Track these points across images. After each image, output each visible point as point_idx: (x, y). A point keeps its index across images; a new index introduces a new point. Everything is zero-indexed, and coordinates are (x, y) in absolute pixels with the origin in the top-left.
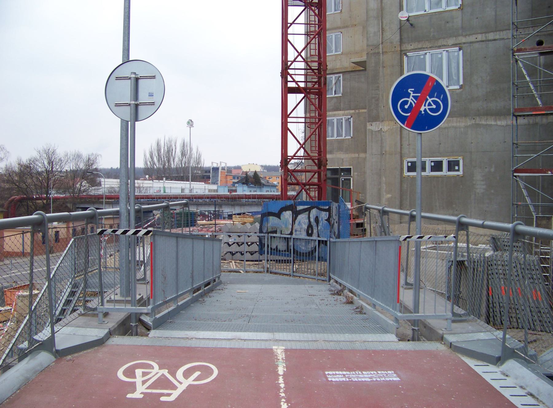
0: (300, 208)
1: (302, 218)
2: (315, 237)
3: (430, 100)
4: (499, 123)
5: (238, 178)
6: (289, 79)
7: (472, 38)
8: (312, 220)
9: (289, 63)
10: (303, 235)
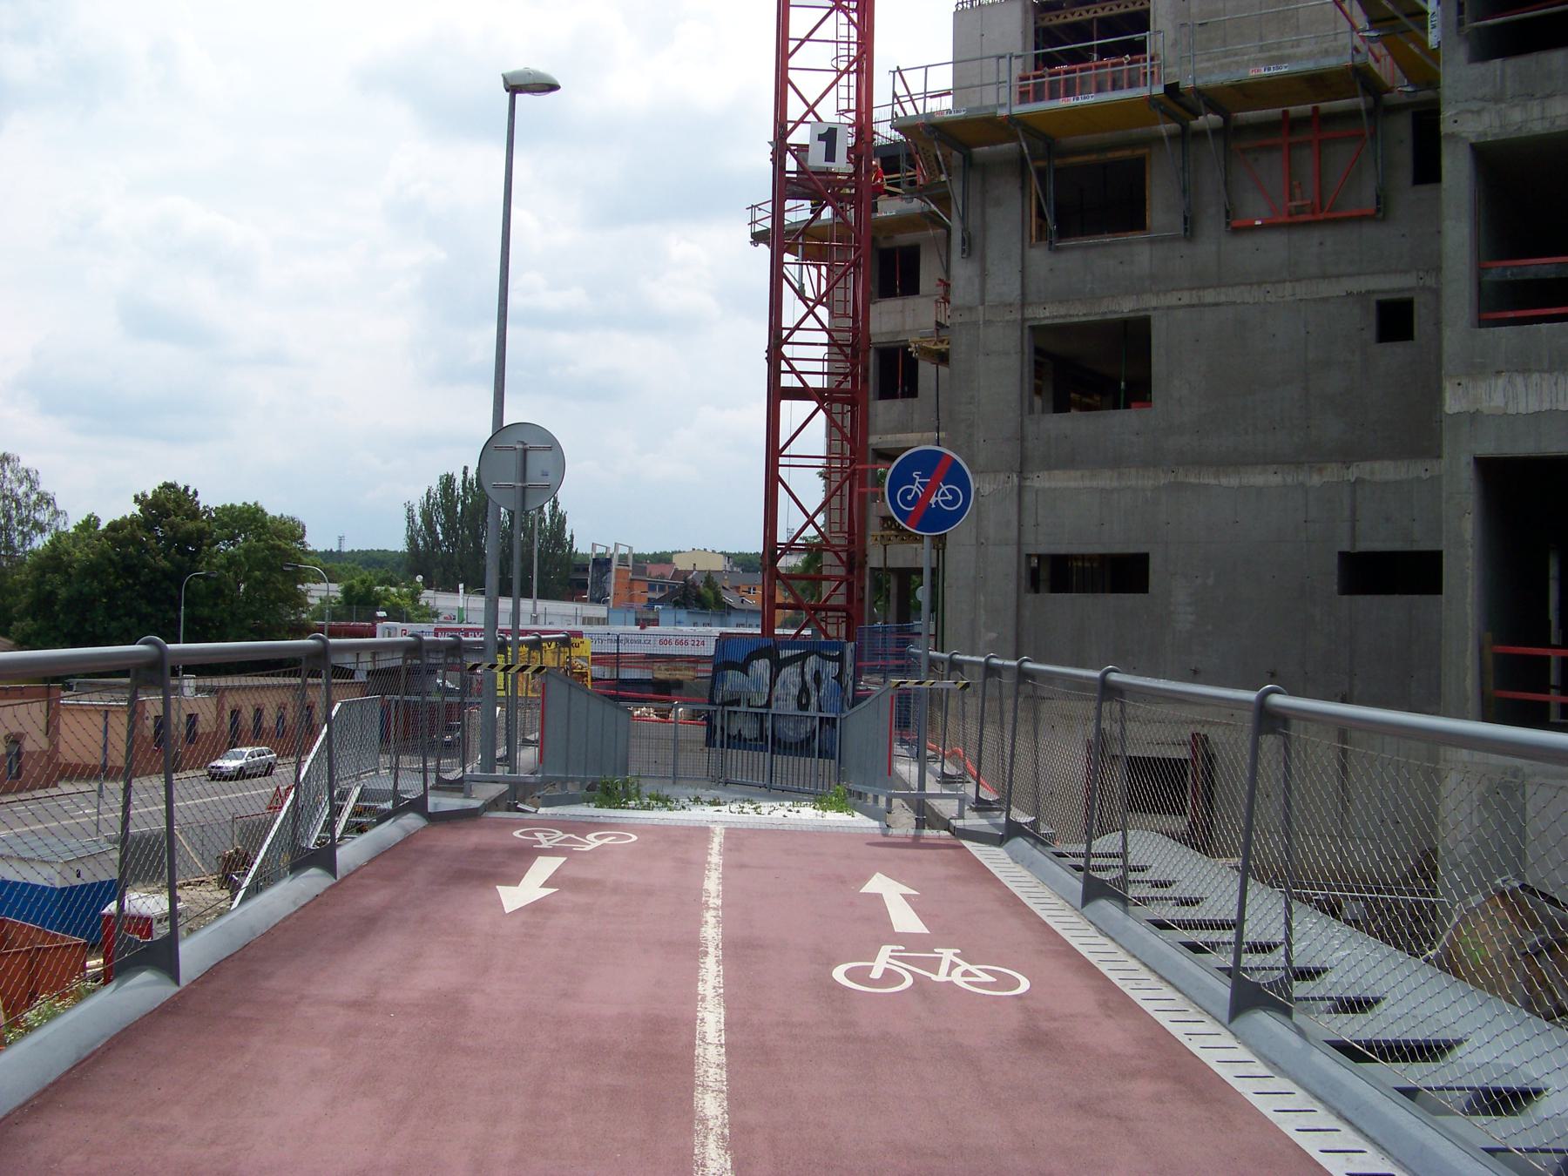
0: (785, 654)
1: (790, 674)
2: (812, 711)
3: (944, 488)
4: (1224, 481)
5: (662, 589)
6: (784, 366)
7: (1171, 299)
8: (808, 678)
9: (785, 333)
10: (791, 707)
